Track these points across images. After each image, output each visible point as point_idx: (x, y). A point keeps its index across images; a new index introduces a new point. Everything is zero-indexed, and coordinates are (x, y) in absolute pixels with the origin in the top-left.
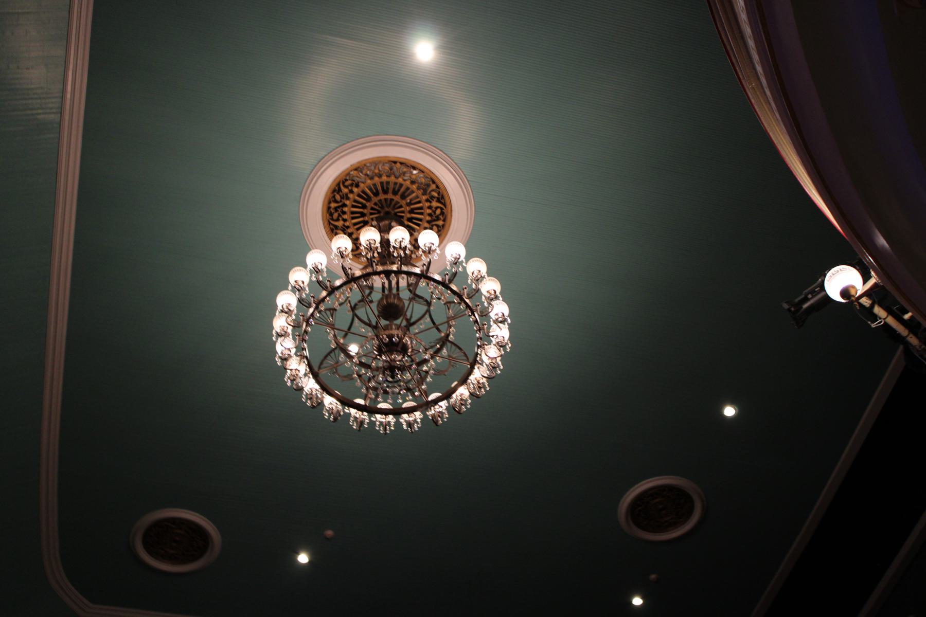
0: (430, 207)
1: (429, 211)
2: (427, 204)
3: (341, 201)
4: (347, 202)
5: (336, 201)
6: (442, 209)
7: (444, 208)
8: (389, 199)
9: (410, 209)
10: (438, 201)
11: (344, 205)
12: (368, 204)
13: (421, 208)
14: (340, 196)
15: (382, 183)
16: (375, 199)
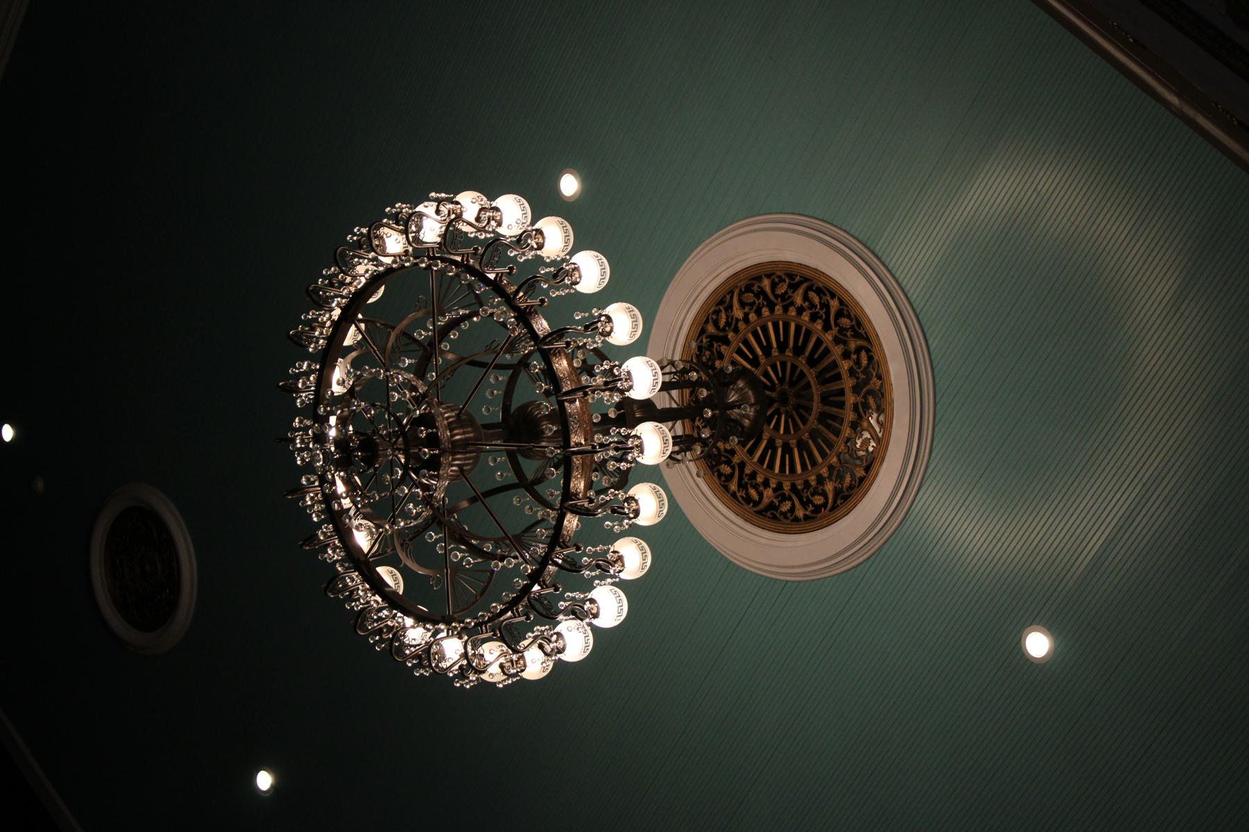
0: (820, 480)
1: (812, 479)
2: (824, 472)
3: (776, 297)
4: (778, 309)
5: (774, 286)
6: (825, 505)
7: (828, 508)
8: (842, 387)
9: (778, 445)
10: (837, 492)
11: (771, 307)
12: (789, 353)
13: (814, 463)
14: (786, 292)
15: (834, 365)
16: (802, 362)
